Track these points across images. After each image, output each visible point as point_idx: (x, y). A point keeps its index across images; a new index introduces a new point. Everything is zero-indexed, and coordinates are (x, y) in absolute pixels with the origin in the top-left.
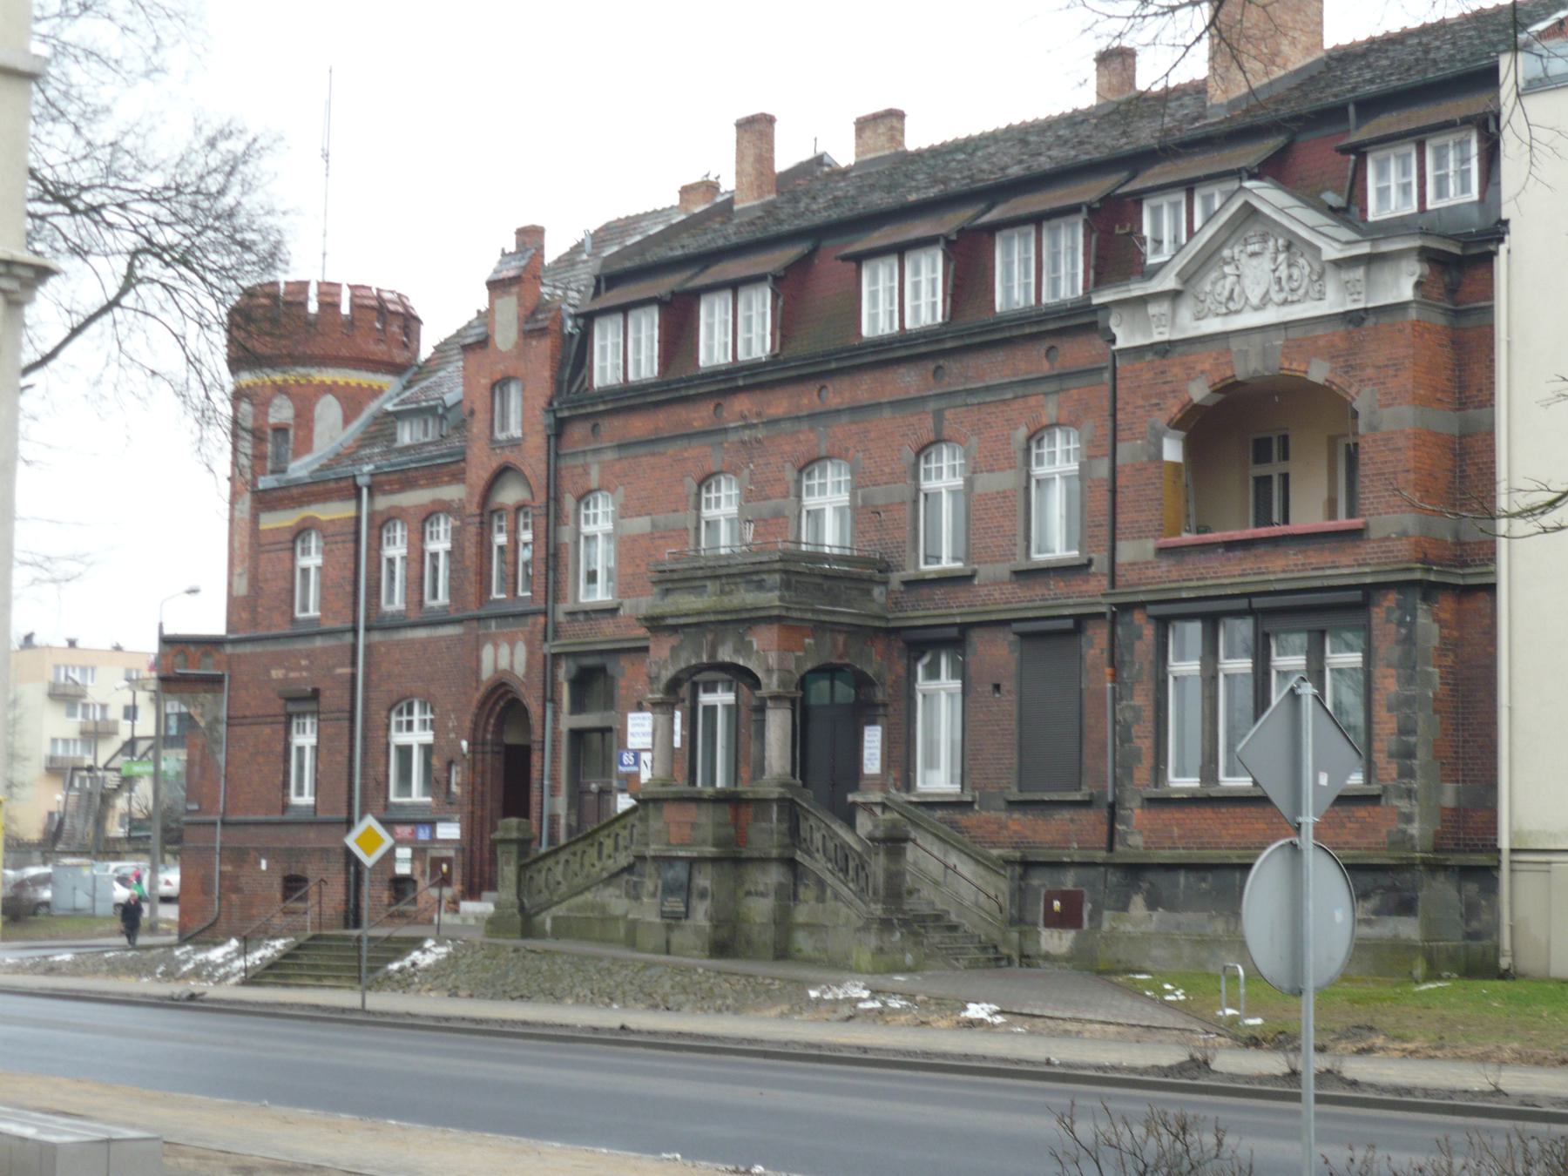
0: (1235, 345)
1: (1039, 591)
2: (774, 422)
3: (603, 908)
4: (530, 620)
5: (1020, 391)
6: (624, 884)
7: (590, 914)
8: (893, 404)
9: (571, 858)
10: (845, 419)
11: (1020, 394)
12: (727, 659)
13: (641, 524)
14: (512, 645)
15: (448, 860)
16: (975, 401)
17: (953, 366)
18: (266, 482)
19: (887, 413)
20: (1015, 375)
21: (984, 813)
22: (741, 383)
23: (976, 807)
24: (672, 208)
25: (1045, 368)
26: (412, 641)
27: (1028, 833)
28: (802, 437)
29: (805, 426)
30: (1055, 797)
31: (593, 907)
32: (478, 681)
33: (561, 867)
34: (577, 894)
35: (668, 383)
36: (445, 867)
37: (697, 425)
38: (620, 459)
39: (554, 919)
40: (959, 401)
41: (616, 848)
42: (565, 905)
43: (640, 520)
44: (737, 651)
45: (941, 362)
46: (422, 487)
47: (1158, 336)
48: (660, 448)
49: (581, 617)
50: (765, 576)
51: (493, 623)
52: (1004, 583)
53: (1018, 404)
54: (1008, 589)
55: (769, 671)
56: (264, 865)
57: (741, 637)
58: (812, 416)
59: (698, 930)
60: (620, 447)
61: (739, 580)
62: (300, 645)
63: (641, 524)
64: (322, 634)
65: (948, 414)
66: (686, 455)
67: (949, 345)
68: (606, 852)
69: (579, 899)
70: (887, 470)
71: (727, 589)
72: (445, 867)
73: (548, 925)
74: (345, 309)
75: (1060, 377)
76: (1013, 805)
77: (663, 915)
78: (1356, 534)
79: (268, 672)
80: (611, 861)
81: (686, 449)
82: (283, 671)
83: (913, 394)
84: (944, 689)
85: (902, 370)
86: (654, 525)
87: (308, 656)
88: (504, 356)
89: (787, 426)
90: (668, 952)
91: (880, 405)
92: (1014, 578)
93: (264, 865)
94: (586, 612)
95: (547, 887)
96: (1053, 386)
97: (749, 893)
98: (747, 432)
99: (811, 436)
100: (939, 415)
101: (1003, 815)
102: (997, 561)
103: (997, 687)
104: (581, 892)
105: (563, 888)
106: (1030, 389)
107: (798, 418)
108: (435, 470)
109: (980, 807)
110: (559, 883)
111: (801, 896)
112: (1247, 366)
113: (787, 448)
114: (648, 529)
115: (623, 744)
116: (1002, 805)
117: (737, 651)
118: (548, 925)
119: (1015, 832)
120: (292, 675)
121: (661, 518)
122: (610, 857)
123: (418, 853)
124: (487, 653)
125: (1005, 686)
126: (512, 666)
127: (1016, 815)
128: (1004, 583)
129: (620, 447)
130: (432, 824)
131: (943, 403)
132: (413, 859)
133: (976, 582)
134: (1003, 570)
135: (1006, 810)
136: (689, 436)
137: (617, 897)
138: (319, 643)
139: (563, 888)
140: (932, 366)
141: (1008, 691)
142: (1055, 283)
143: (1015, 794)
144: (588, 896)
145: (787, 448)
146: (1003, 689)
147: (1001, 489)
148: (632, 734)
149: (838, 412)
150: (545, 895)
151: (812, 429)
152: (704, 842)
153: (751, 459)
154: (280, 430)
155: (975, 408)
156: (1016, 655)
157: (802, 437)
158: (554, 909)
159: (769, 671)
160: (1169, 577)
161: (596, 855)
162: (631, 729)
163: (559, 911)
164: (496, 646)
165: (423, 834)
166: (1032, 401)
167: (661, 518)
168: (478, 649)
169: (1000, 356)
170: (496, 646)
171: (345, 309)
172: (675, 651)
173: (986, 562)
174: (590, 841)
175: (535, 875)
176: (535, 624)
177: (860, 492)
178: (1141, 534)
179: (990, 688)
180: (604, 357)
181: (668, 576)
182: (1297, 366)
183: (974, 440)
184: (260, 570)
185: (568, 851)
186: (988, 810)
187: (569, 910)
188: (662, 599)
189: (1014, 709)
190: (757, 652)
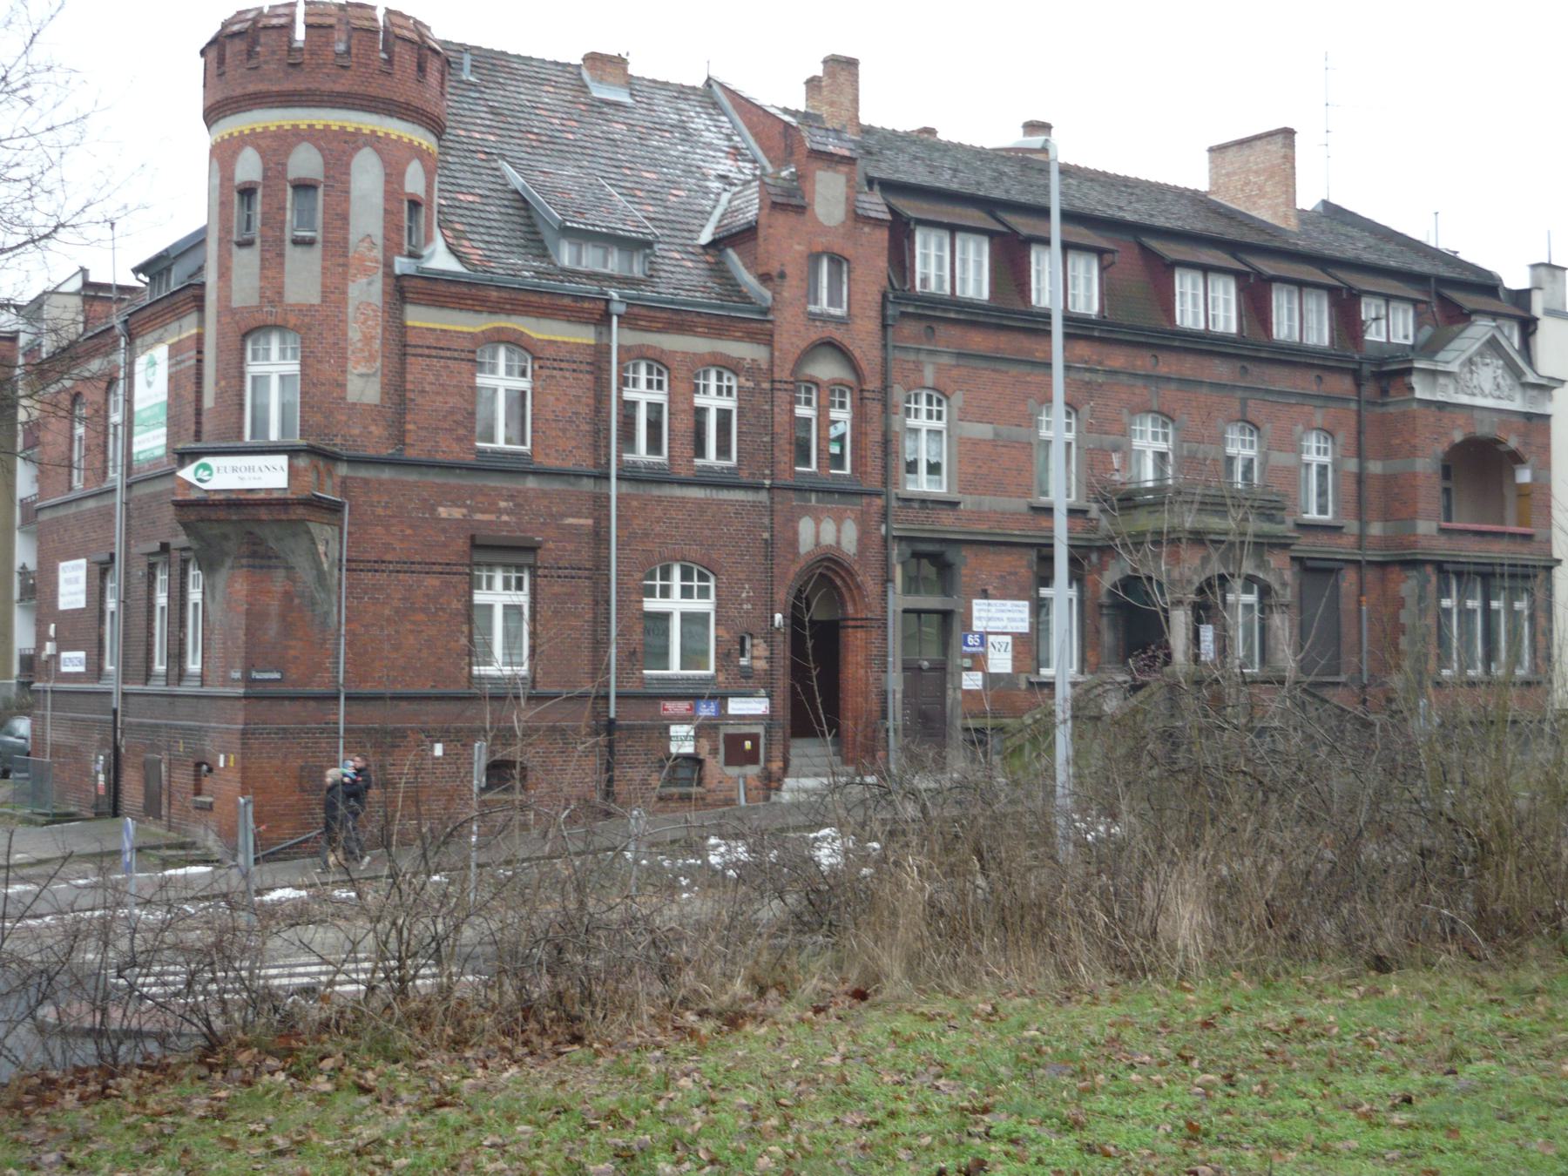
0: (1477, 414)
1: (1311, 540)
2: (1112, 372)
4: (865, 500)
10: (1173, 386)
13: (983, 431)
14: (839, 521)
15: (754, 738)
17: (1254, 369)
18: (402, 265)
19: (1205, 390)
24: (694, 88)
25: (1313, 389)
26: (683, 500)
29: (1140, 383)
32: (796, 553)
35: (997, 309)
36: (748, 745)
38: (958, 366)
43: (980, 426)
44: (1258, 567)
46: (696, 334)
47: (1440, 397)
48: (1003, 367)
49: (916, 505)
51: (813, 497)
55: (1284, 585)
56: (438, 750)
58: (1147, 377)
60: (960, 355)
62: (494, 482)
63: (983, 431)
64: (539, 473)
65: (1251, 403)
67: (1264, 355)
72: (748, 745)
74: (300, 33)
78: (1528, 537)
79: (433, 509)
82: (464, 511)
85: (1217, 361)
86: (997, 434)
87: (511, 497)
88: (826, 230)
89: (1124, 378)
91: (1201, 383)
93: (438, 750)
94: (923, 501)
96: (1318, 403)
100: (1244, 402)
108: (727, 322)
112: (1484, 429)
113: (1124, 396)
114: (990, 436)
115: (967, 626)
117: (1258, 567)
120: (479, 516)
121: (1005, 430)
123: (704, 730)
124: (806, 527)
126: (838, 543)
129: (960, 355)
130: (722, 698)
131: (1247, 394)
132: (697, 737)
138: (531, 483)
140: (1239, 364)
145: (1124, 396)
151: (1145, 387)
153: (1092, 397)
154: (304, 187)
159: (1284, 585)
160: (1443, 548)
162: (975, 614)
164: (818, 522)
165: (707, 710)
166: (1306, 409)
167: (1005, 430)
168: (792, 522)
170: (818, 522)
171: (300, 33)
176: (869, 505)
178: (1428, 518)
180: (925, 264)
182: (1502, 435)
184: (409, 377)
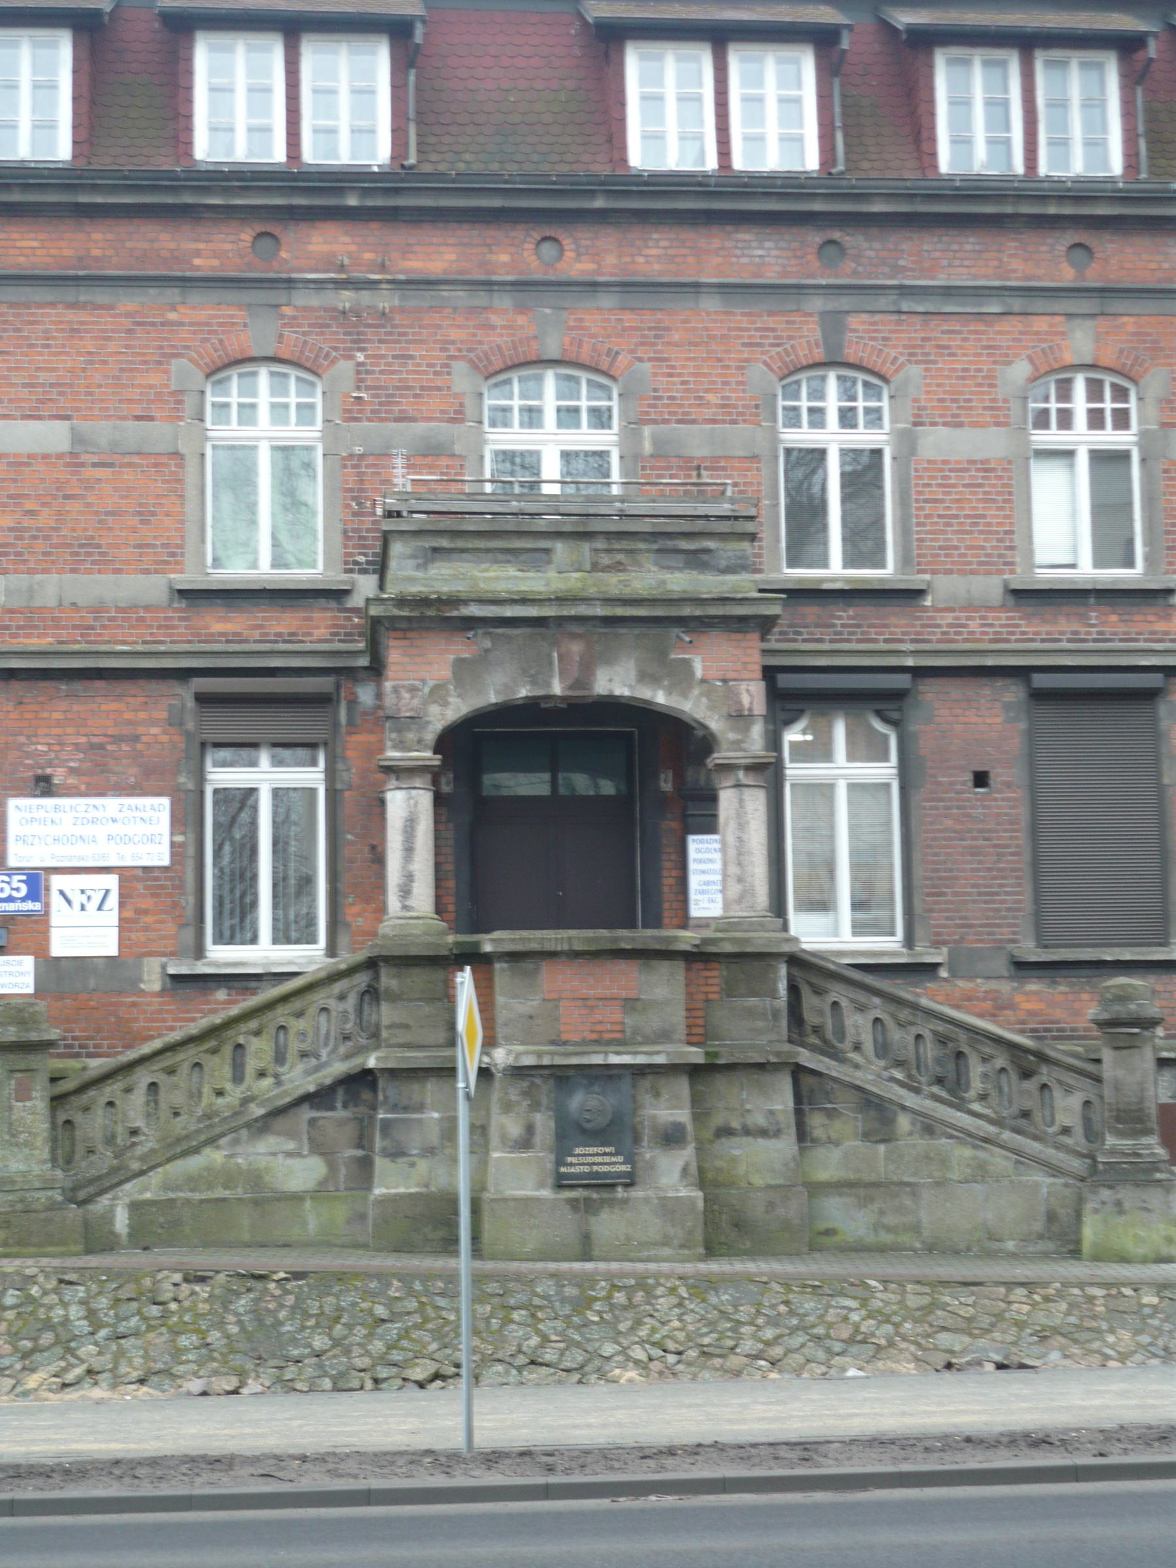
3: (255, 1179)
5: (1017, 304)
6: (304, 1127)
7: (221, 1193)
8: (725, 289)
9: (161, 1078)
11: (1016, 309)
12: (621, 690)
16: (921, 309)
20: (1001, 278)
21: (961, 983)
22: (352, 201)
23: (943, 973)
25: (1066, 275)
27: (1058, 1014)
28: (495, 319)
29: (504, 301)
30: (1127, 955)
31: (229, 1178)
33: (139, 1097)
34: (185, 1154)
37: (204, 264)
39: (135, 1207)
40: (883, 302)
41: (280, 1058)
42: (155, 1178)
45: (836, 235)
50: (711, 544)
52: (990, 609)
53: (1013, 325)
54: (1000, 620)
55: (740, 718)
57: (661, 655)
59: (668, 1208)
61: (641, 546)
65: (853, 321)
66: (172, 316)
68: (252, 1065)
69: (194, 1163)
70: (712, 398)
71: (605, 560)
73: (121, 1221)
75: (1105, 292)
76: (1022, 967)
77: (561, 1182)
80: (267, 1082)
81: (173, 308)
83: (771, 277)
84: (844, 777)
86: (77, 438)
90: (586, 1256)
91: (696, 288)
92: (1011, 601)
95: (110, 1140)
97: (725, 1132)
98: (347, 294)
99: (521, 320)
100: (833, 323)
101: (1005, 987)
102: (973, 572)
103: (981, 779)
104: (196, 1150)
105: (148, 1143)
106: (1039, 305)
107: (489, 285)
109: (950, 970)
110: (134, 1132)
111: (818, 1133)
114: (64, 446)
116: (1001, 966)
117: (644, 677)
118: (121, 1221)
119: (1032, 1013)
121: (103, 431)
122: (262, 1074)
125: (998, 776)
127: (1033, 986)
128: (990, 609)
133: (928, 602)
134: (990, 587)
135: (1011, 978)
136: (186, 283)
137: (290, 1154)
139: (148, 1143)
141: (1008, 785)
142: (1061, 143)
143: (1030, 951)
144: (214, 1157)
146: (994, 780)
147: (978, 456)
148: (18, 838)
149: (592, 286)
150: (105, 1160)
151: (521, 309)
152: (664, 1036)
153: (359, 344)
155: (917, 319)
156: (1022, 725)
157: (495, 319)
158: (128, 1186)
161: (227, 1071)
163: (149, 1188)
166: (1041, 324)
167: (103, 431)
169: (970, 242)
172: (465, 672)
173: (949, 572)
174: (212, 1043)
175: (78, 1118)
177: (647, 431)
179: (969, 777)
181: (446, 523)
183: (915, 371)
185: (158, 1065)
186: (971, 978)
187: (166, 1187)
188: (423, 566)
189: (1023, 813)
190: (703, 681)
